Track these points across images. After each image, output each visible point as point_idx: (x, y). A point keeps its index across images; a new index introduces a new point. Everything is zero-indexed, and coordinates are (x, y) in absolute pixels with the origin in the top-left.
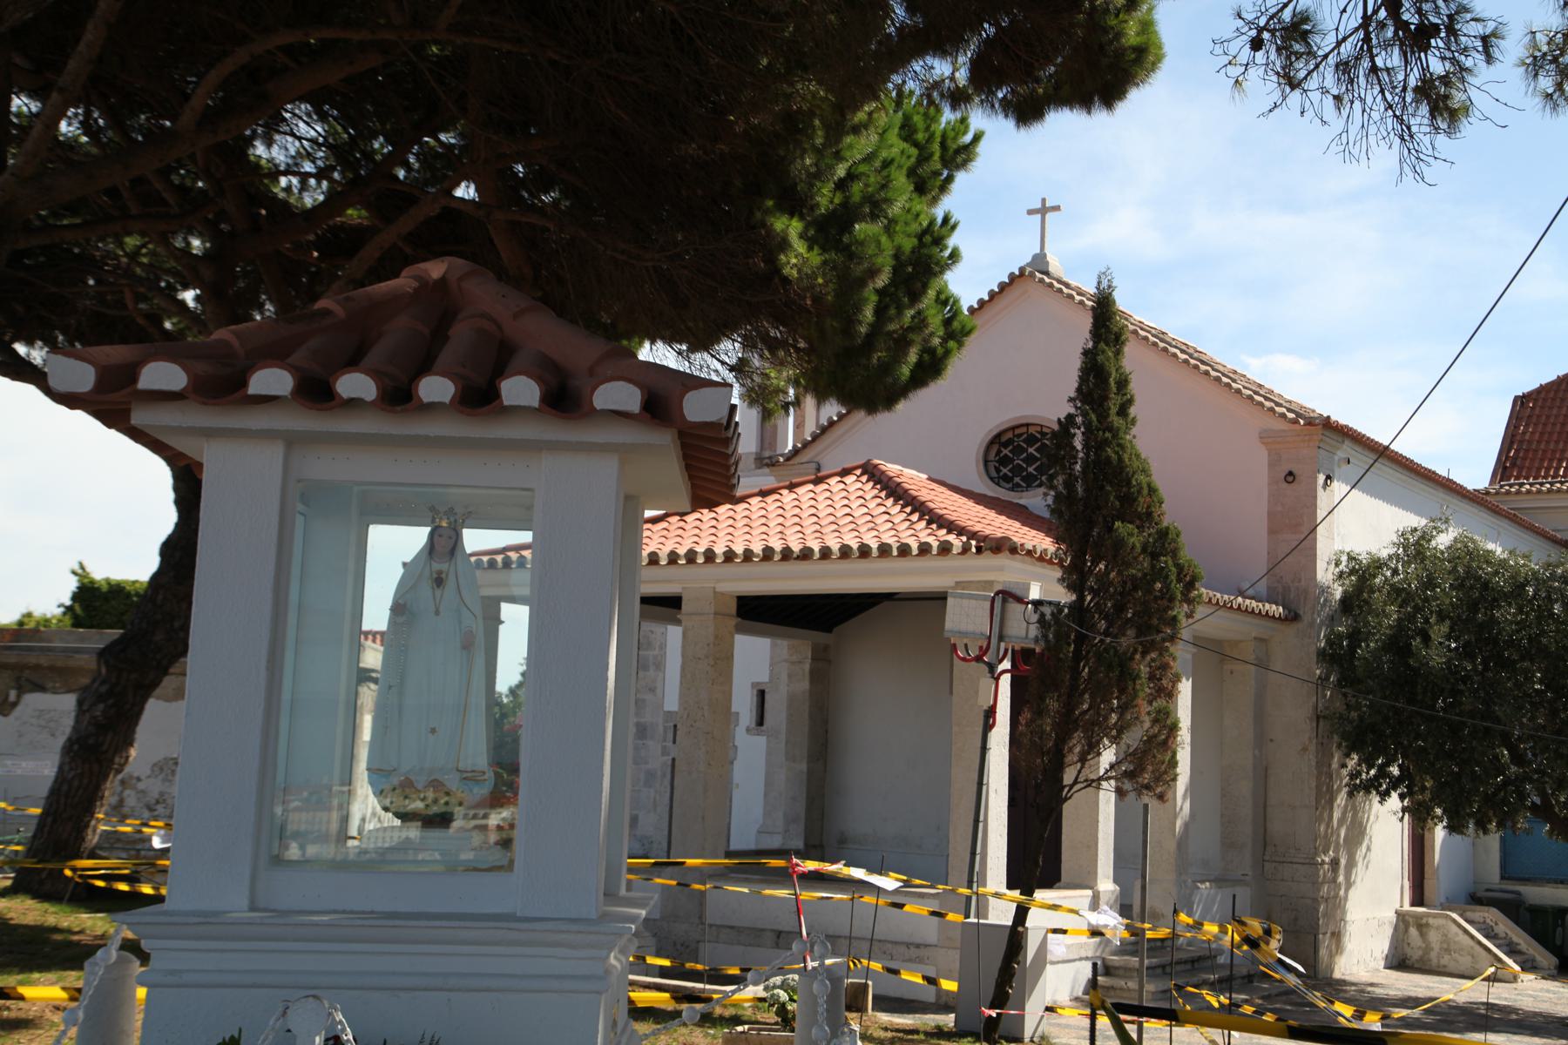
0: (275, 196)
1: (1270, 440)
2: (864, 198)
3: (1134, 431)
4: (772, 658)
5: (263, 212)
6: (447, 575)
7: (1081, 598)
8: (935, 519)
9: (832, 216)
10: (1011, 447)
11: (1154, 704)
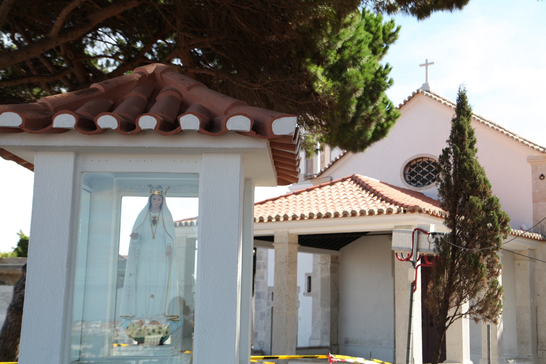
0: (96, 69)
1: (532, 161)
2: (350, 57)
3: (477, 155)
4: (314, 262)
5: (91, 75)
6: (158, 219)
7: (454, 231)
8: (384, 199)
9: (336, 65)
10: (415, 168)
11: (490, 279)
